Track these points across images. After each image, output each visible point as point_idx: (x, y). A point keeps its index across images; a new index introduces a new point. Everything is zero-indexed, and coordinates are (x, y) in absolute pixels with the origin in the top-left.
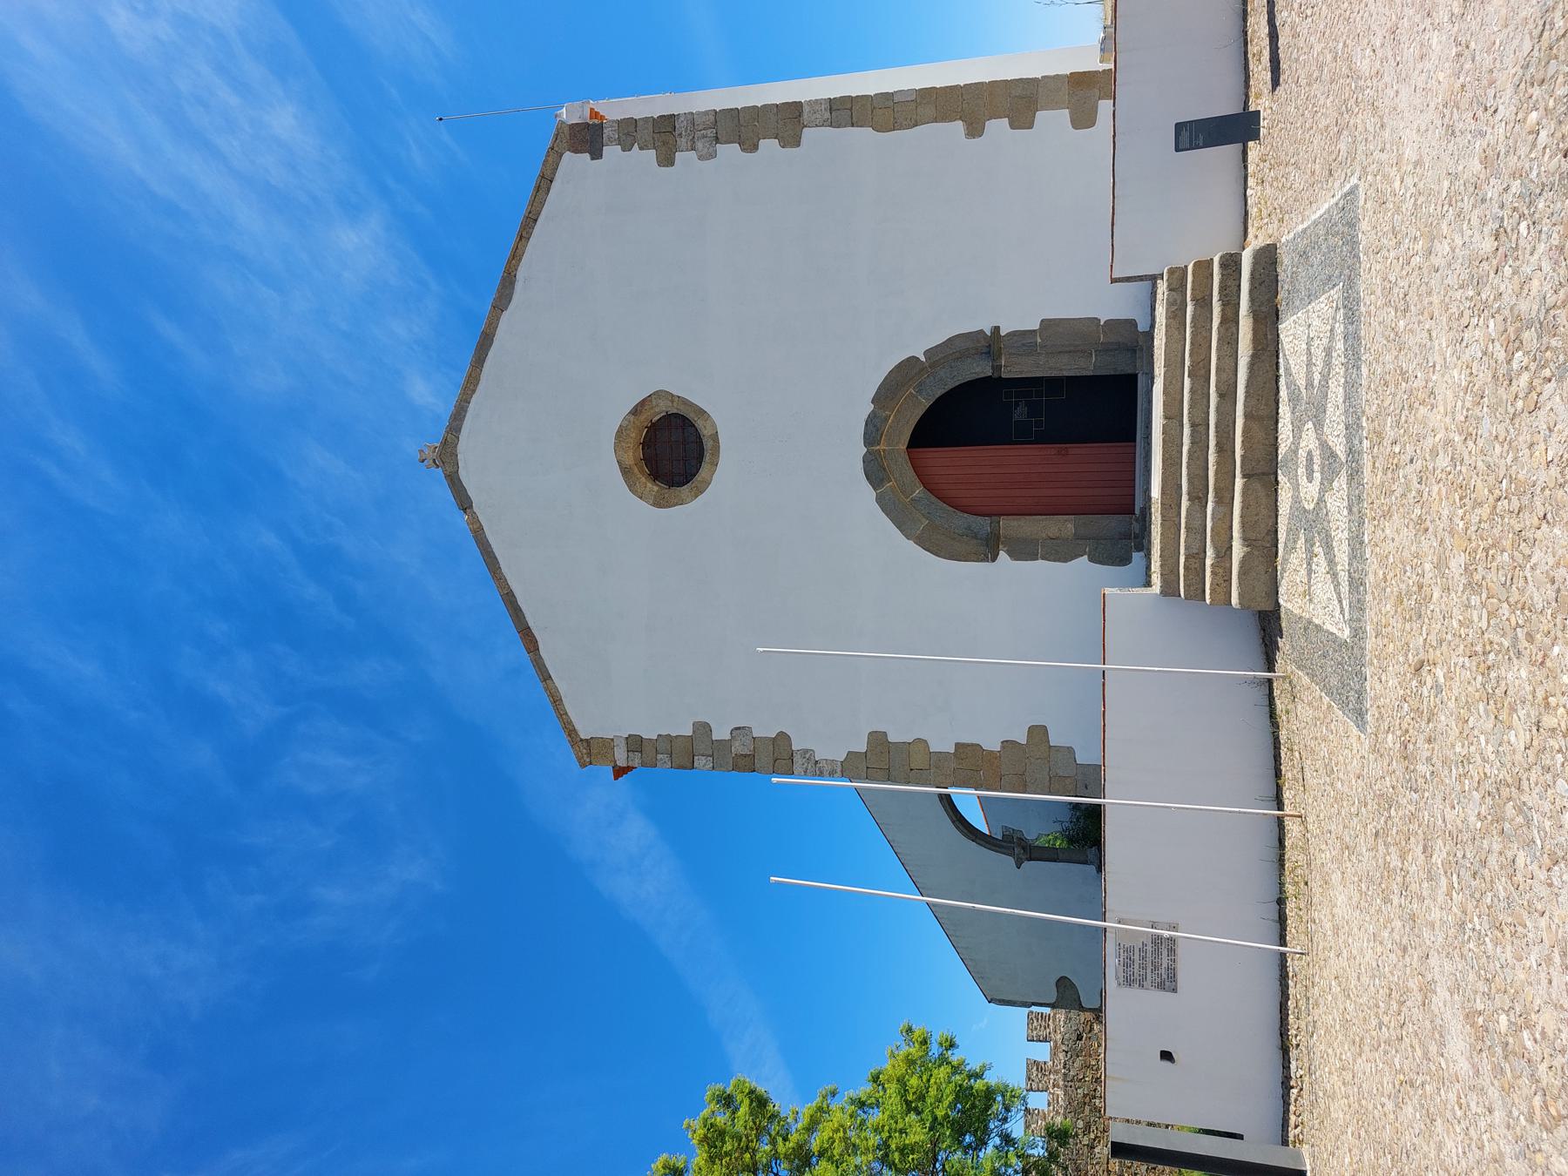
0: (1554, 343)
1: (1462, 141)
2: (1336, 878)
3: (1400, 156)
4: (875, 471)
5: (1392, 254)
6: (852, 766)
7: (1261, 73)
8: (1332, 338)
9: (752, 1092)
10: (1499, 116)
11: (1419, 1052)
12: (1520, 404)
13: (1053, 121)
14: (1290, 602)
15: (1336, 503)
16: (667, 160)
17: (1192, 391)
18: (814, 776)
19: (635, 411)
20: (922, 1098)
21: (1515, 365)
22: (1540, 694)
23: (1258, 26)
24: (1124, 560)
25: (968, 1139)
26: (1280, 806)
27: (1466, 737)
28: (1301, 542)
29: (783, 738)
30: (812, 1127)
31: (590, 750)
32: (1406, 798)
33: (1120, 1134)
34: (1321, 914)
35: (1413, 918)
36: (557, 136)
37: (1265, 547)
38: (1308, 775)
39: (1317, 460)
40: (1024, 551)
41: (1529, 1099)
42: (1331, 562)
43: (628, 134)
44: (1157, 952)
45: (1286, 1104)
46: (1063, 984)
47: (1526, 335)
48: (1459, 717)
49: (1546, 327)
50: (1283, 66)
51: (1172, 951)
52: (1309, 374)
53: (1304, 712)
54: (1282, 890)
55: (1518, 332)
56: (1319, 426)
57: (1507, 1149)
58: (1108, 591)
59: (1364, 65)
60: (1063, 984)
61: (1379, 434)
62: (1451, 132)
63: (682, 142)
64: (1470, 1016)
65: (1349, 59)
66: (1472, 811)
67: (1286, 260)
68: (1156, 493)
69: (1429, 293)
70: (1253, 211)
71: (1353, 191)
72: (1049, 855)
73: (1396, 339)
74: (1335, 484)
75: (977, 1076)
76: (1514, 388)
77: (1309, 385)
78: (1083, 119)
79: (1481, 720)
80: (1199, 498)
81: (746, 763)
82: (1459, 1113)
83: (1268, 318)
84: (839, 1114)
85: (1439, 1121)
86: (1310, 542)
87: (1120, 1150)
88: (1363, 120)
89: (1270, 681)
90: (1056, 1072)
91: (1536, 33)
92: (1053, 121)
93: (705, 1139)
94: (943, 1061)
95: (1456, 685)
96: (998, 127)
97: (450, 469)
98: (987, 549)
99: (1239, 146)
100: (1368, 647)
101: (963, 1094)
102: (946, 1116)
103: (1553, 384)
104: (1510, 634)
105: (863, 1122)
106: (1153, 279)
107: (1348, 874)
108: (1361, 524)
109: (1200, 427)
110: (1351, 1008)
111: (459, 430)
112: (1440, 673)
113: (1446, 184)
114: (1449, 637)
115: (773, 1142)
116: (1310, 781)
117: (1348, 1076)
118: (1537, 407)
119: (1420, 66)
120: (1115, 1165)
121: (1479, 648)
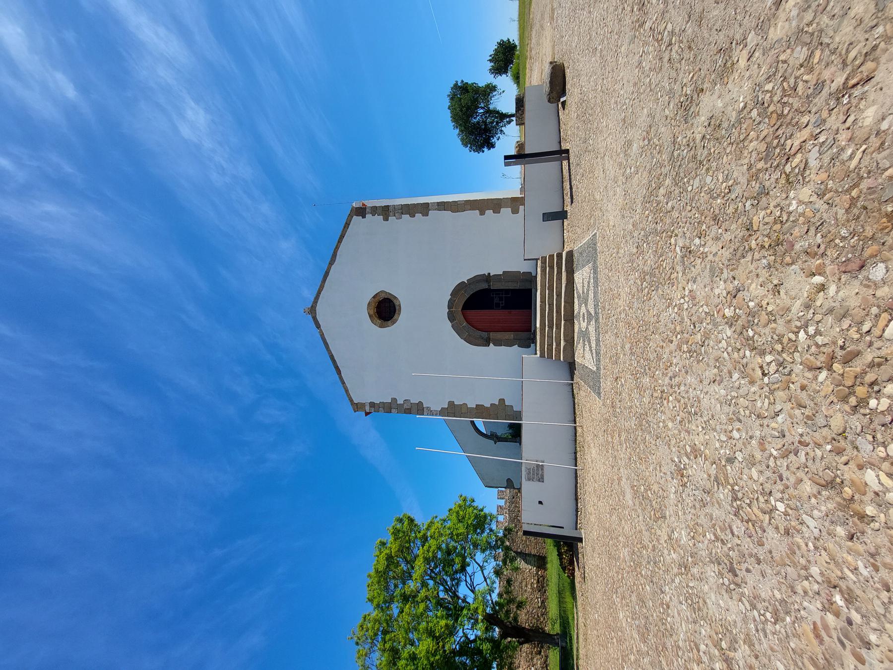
0: (655, 279)
1: (627, 219)
2: (592, 445)
3: (609, 224)
4: (451, 317)
5: (607, 253)
6: (443, 412)
7: (567, 199)
8: (590, 279)
9: (409, 517)
10: (637, 212)
11: (617, 499)
12: (645, 298)
13: (506, 211)
14: (578, 359)
15: (592, 329)
16: (386, 219)
17: (549, 294)
18: (430, 415)
19: (374, 297)
20: (463, 518)
21: (644, 286)
22: (653, 386)
23: (567, 185)
24: (529, 346)
25: (478, 531)
26: (575, 423)
27: (631, 400)
28: (581, 341)
29: (420, 403)
30: (428, 529)
31: (357, 407)
32: (613, 419)
33: (526, 528)
34: (588, 457)
35: (615, 457)
36: (351, 211)
37: (570, 342)
38: (584, 413)
39: (586, 316)
40: (498, 343)
41: (650, 513)
42: (590, 347)
43: (374, 211)
44: (538, 470)
45: (577, 517)
46: (509, 481)
47: (647, 277)
48: (629, 394)
49: (652, 275)
50: (574, 197)
51: (542, 469)
52: (583, 289)
53: (582, 393)
54: (576, 450)
55: (644, 276)
56: (586, 305)
57: (643, 528)
58: (523, 356)
59: (598, 197)
60: (509, 481)
61: (604, 307)
62: (623, 216)
63: (391, 214)
64: (632, 487)
65: (594, 195)
66: (633, 423)
67: (576, 255)
68: (538, 325)
69: (618, 265)
70: (566, 240)
71: (595, 234)
72: (505, 440)
73: (609, 279)
74: (591, 323)
75: (482, 510)
76: (643, 293)
77: (583, 292)
78: (515, 211)
79: (635, 395)
80: (551, 327)
81: (408, 411)
82: (629, 518)
83: (571, 272)
84: (437, 525)
85: (623, 521)
86: (584, 341)
87: (526, 533)
88: (598, 213)
89: (572, 384)
90: (506, 509)
91: (647, 188)
92: (506, 211)
93: (393, 533)
94: (470, 506)
95: (627, 384)
96: (489, 213)
97: (313, 315)
98: (486, 343)
99: (562, 221)
100: (602, 373)
101: (476, 516)
102: (472, 523)
103: (655, 292)
104: (644, 368)
105: (445, 527)
106: (537, 260)
107: (596, 444)
108: (599, 335)
109: (551, 305)
110: (596, 486)
111: (317, 302)
112: (623, 381)
113: (622, 232)
114: (626, 369)
115: (415, 533)
116: (584, 415)
117: (596, 507)
118: (650, 299)
119: (614, 198)
120: (524, 538)
121: (634, 373)
